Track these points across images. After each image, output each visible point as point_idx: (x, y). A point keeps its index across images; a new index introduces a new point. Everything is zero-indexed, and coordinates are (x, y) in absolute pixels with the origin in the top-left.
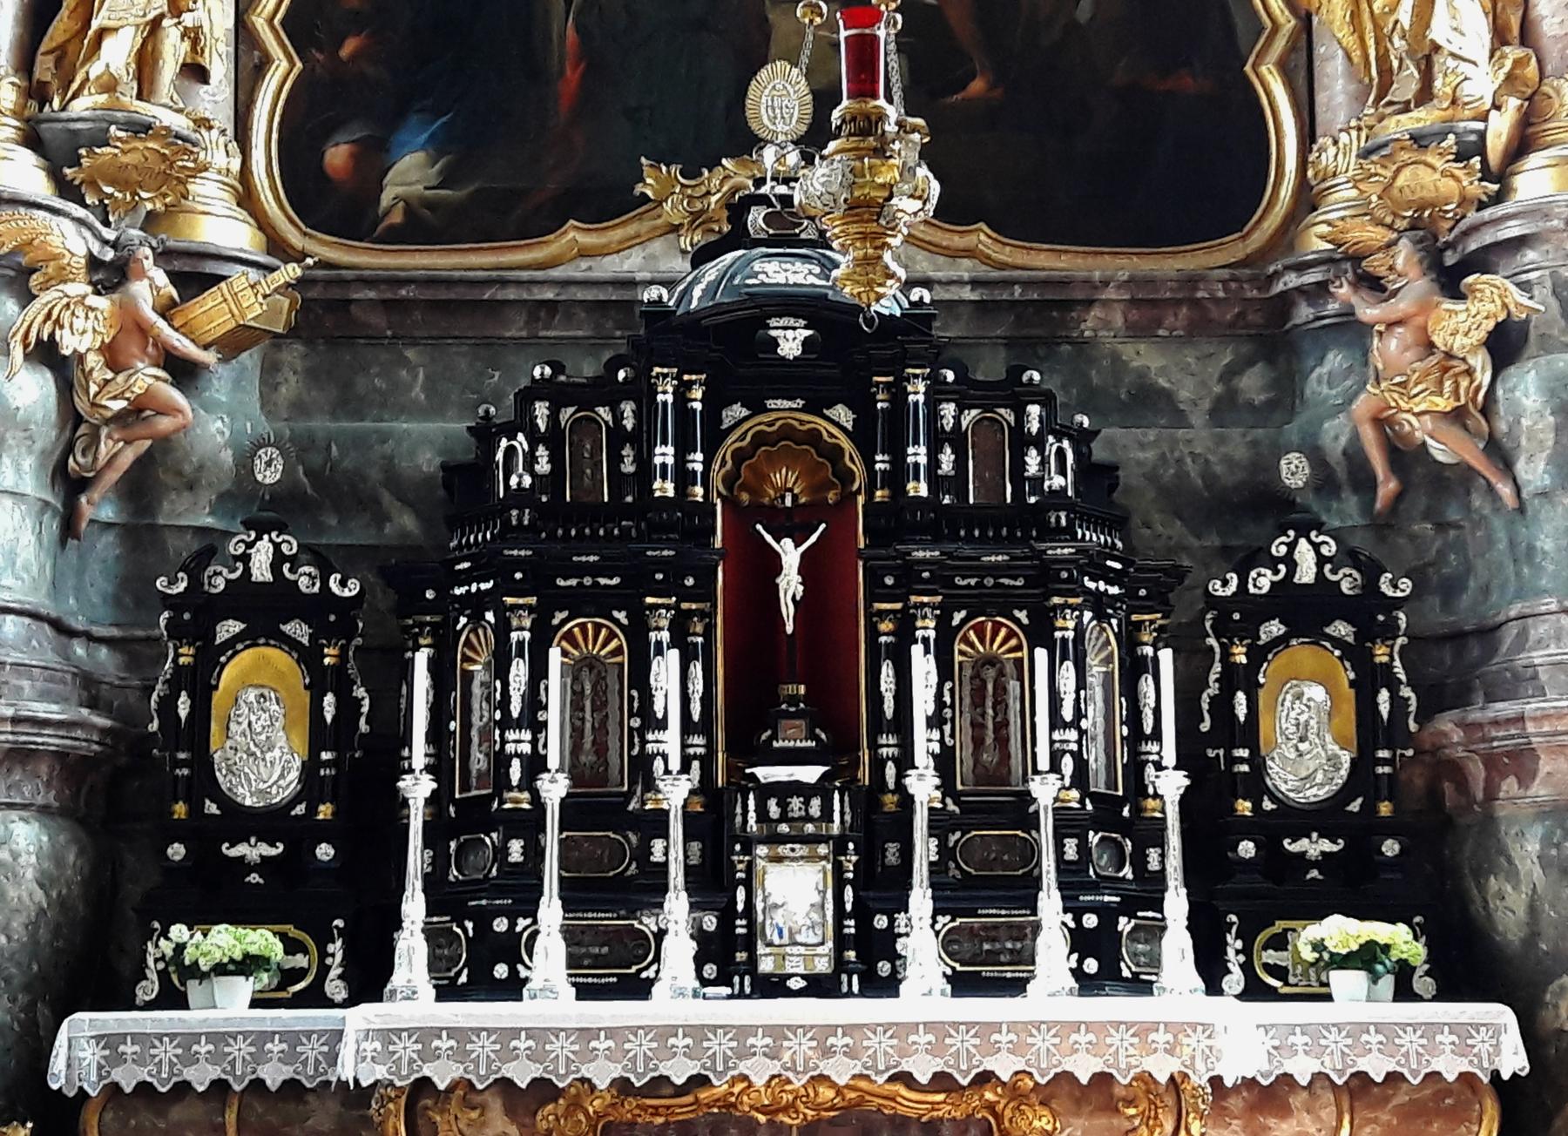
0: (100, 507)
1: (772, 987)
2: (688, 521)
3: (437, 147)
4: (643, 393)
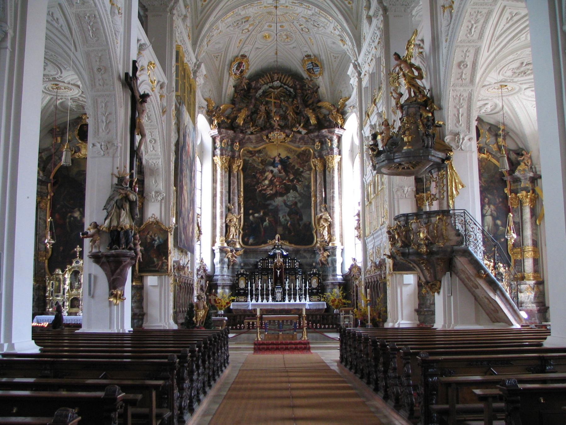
0: (230, 267)
1: (277, 301)
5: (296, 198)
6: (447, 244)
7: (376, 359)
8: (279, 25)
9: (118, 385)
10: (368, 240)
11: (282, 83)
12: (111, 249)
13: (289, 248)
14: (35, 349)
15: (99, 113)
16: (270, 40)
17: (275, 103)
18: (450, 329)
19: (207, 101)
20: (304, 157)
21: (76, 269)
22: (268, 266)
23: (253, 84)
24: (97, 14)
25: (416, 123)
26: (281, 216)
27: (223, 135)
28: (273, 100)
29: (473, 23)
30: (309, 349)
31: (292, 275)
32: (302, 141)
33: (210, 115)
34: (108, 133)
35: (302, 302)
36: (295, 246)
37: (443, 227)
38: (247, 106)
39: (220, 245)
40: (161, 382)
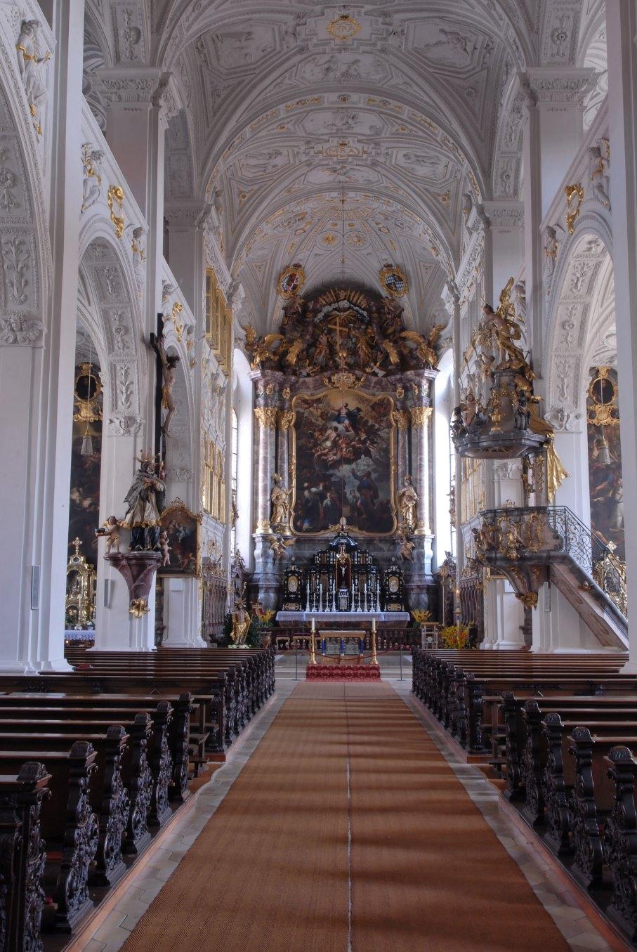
0: (277, 562)
1: (341, 611)
2: (334, 565)
3: (309, 522)
5: (369, 466)
6: (542, 548)
7: (440, 684)
8: (346, 223)
9: (148, 713)
10: (465, 529)
11: (351, 303)
12: (133, 549)
13: (358, 535)
14: (67, 667)
15: (118, 382)
16: (335, 242)
17: (341, 331)
18: (548, 653)
19: (246, 330)
20: (381, 408)
21: (75, 568)
22: (329, 561)
23: (311, 305)
24: (118, 266)
25: (509, 395)
26: (348, 491)
27: (268, 378)
28: (338, 328)
29: (578, 275)
30: (379, 675)
31: (363, 574)
32: (378, 386)
33: (251, 349)
34: (129, 407)
35: (371, 612)
36: (368, 534)
37: (539, 528)
38: (302, 336)
39: (262, 531)
40: (212, 697)
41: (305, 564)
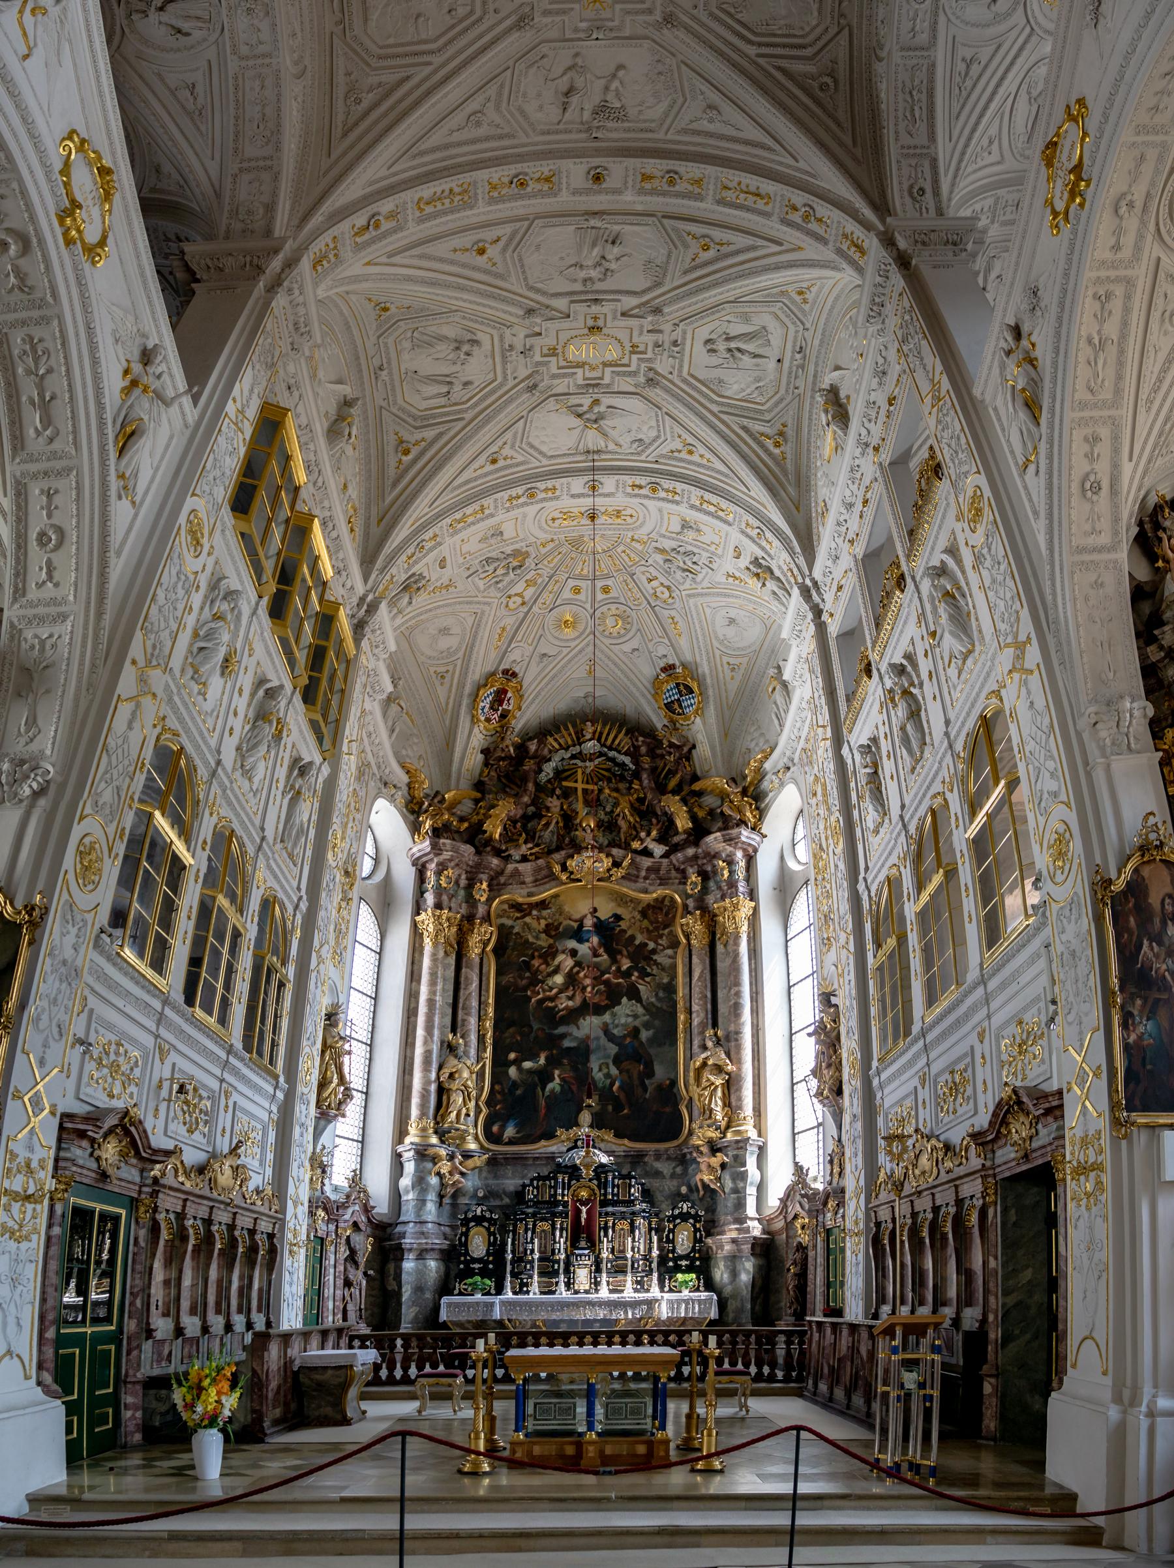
0: (447, 1200)
3: (516, 1126)
4: (556, 1179)
5: (635, 1016)
13: (614, 1148)
17: (585, 791)
20: (659, 915)
23: (533, 746)
26: (594, 1064)
28: (580, 786)
33: (413, 810)
39: (417, 1140)
41: (507, 1206)
